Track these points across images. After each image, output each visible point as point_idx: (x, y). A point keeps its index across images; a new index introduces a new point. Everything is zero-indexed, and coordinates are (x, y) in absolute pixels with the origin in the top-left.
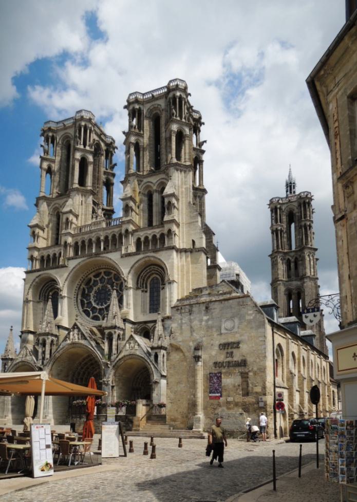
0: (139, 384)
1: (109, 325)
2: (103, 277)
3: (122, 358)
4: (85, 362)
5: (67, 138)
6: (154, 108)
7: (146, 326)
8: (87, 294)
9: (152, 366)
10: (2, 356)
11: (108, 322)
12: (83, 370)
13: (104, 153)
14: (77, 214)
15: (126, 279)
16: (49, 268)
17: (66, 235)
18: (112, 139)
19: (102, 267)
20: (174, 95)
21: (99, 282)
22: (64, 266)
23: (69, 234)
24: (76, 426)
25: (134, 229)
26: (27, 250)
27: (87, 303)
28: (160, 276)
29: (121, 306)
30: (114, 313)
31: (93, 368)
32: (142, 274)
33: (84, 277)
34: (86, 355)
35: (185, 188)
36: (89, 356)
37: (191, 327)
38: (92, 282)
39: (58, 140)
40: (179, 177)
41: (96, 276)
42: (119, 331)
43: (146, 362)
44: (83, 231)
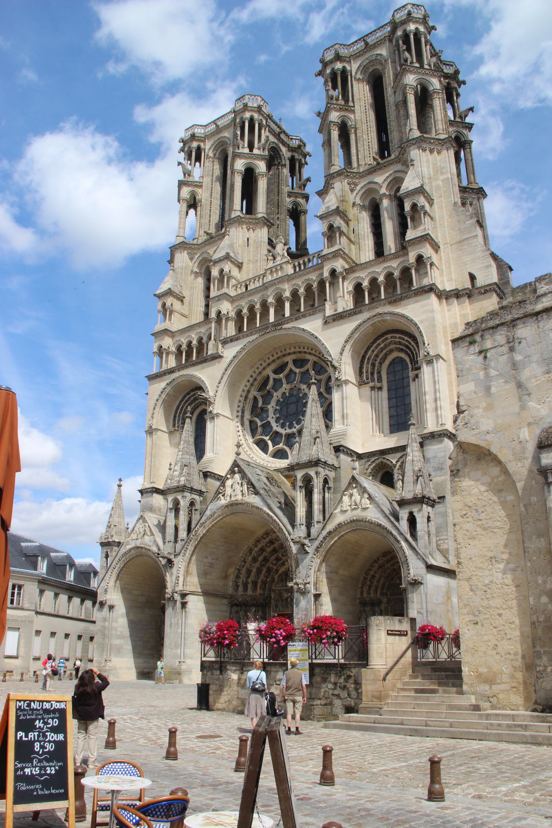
0: (376, 591)
1: (304, 459)
2: (291, 370)
3: (335, 530)
4: (260, 546)
5: (222, 146)
6: (370, 62)
7: (385, 461)
8: (262, 409)
9: (403, 544)
10: (101, 538)
11: (302, 453)
12: (257, 564)
13: (288, 163)
14: (240, 261)
15: (336, 364)
16: (190, 364)
17: (219, 300)
18: (301, 141)
19: (288, 351)
20: (405, 31)
21: (284, 381)
22: (217, 357)
23: (226, 296)
24: (211, 692)
25: (347, 266)
26: (153, 337)
27: (263, 426)
28: (409, 355)
29: (330, 423)
30: (314, 432)
31: (278, 559)
32: (370, 353)
33: (255, 376)
34: (260, 532)
35: (443, 181)
36: (267, 534)
37: (519, 385)
38: (271, 382)
39: (206, 151)
40: (428, 161)
41: (278, 370)
42: (327, 472)
43: (389, 536)
44: (251, 287)
